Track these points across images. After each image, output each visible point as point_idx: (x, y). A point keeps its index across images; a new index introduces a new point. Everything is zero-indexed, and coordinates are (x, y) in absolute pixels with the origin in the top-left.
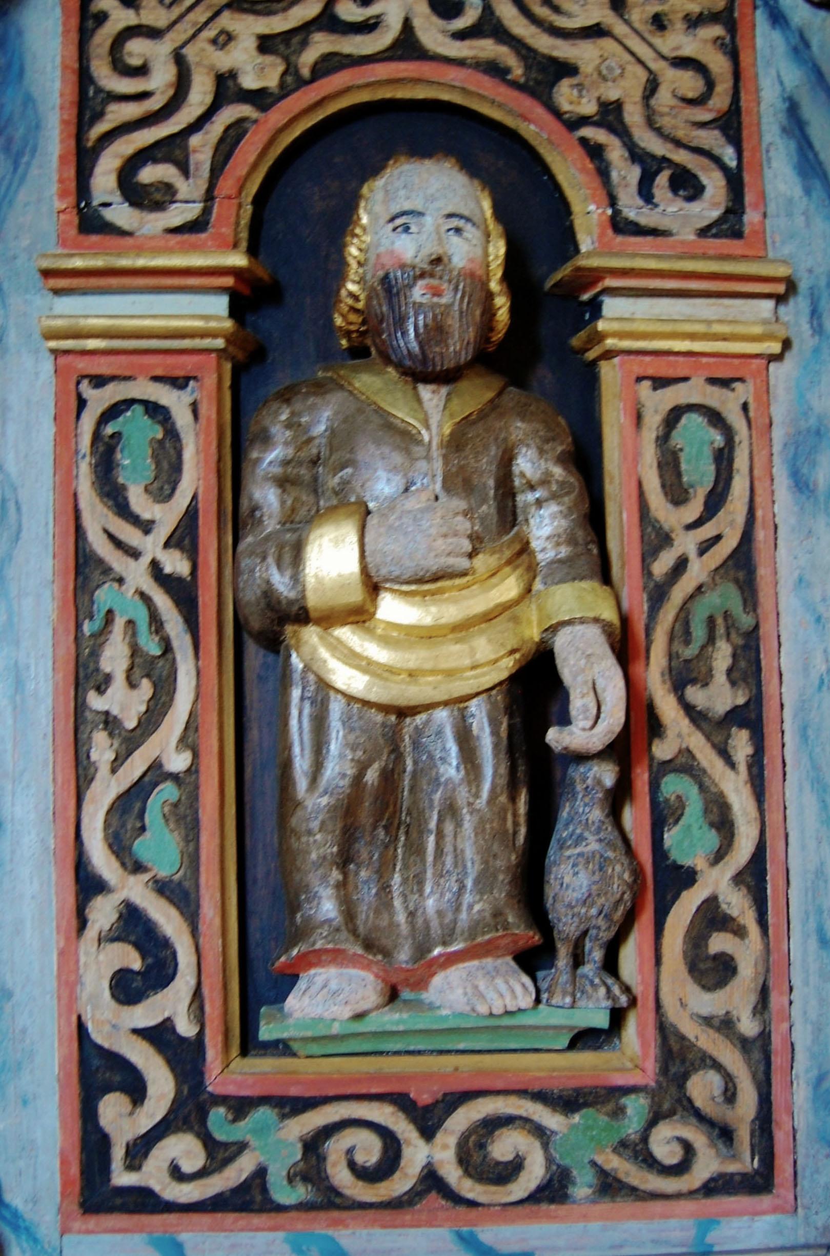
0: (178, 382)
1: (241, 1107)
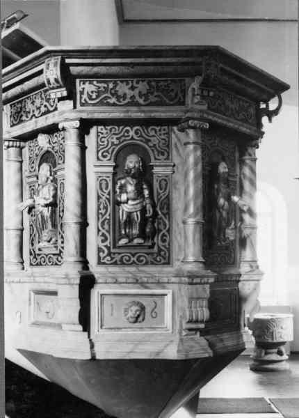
1: (114, 254)
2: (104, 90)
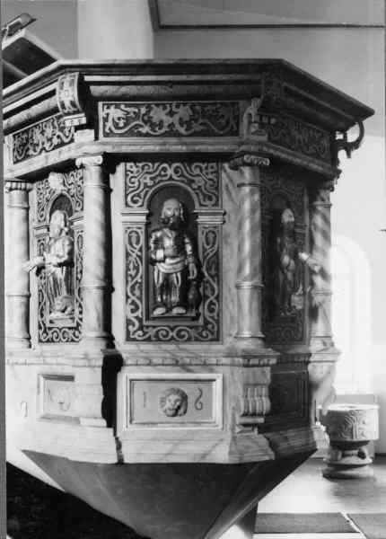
0: (140, 228)
1: (148, 327)
2: (134, 116)
